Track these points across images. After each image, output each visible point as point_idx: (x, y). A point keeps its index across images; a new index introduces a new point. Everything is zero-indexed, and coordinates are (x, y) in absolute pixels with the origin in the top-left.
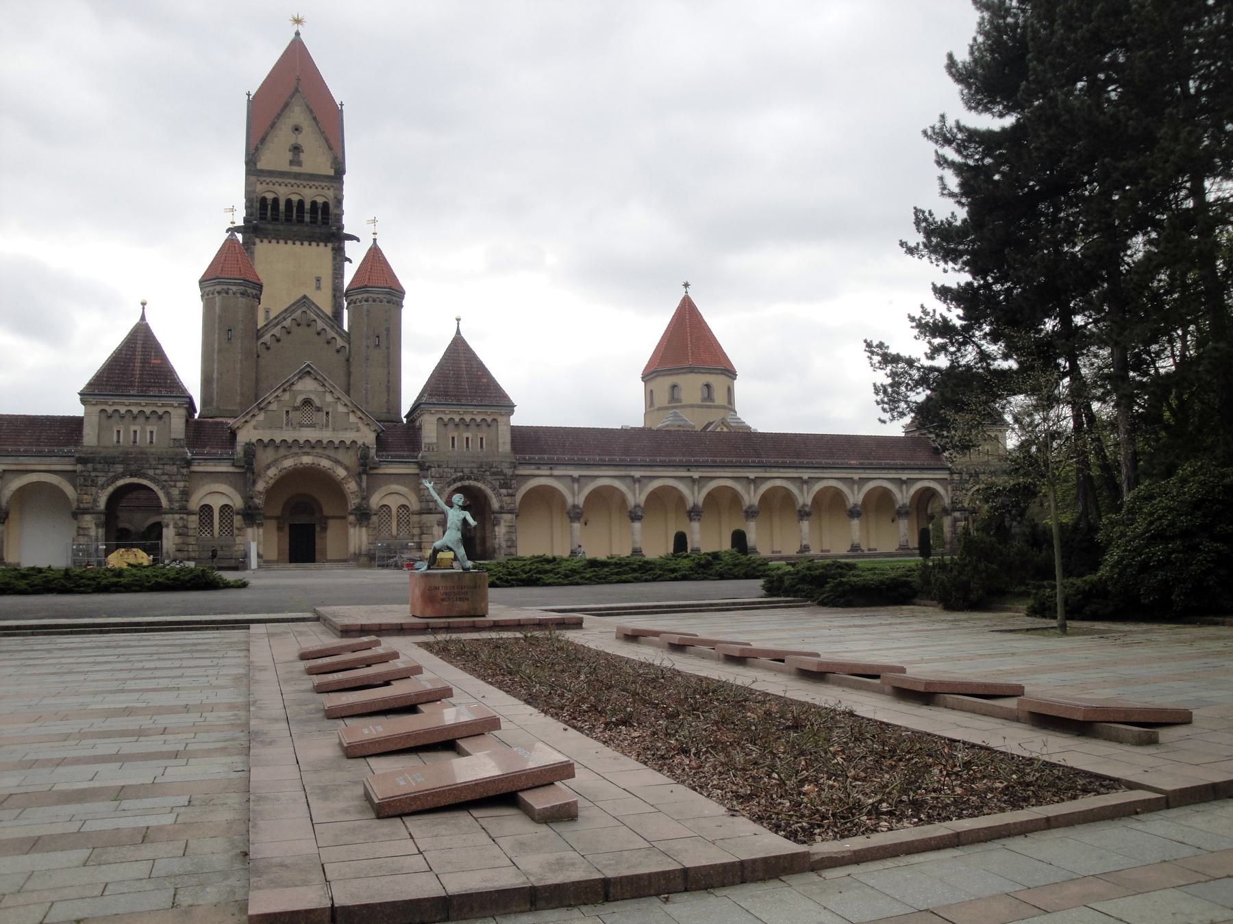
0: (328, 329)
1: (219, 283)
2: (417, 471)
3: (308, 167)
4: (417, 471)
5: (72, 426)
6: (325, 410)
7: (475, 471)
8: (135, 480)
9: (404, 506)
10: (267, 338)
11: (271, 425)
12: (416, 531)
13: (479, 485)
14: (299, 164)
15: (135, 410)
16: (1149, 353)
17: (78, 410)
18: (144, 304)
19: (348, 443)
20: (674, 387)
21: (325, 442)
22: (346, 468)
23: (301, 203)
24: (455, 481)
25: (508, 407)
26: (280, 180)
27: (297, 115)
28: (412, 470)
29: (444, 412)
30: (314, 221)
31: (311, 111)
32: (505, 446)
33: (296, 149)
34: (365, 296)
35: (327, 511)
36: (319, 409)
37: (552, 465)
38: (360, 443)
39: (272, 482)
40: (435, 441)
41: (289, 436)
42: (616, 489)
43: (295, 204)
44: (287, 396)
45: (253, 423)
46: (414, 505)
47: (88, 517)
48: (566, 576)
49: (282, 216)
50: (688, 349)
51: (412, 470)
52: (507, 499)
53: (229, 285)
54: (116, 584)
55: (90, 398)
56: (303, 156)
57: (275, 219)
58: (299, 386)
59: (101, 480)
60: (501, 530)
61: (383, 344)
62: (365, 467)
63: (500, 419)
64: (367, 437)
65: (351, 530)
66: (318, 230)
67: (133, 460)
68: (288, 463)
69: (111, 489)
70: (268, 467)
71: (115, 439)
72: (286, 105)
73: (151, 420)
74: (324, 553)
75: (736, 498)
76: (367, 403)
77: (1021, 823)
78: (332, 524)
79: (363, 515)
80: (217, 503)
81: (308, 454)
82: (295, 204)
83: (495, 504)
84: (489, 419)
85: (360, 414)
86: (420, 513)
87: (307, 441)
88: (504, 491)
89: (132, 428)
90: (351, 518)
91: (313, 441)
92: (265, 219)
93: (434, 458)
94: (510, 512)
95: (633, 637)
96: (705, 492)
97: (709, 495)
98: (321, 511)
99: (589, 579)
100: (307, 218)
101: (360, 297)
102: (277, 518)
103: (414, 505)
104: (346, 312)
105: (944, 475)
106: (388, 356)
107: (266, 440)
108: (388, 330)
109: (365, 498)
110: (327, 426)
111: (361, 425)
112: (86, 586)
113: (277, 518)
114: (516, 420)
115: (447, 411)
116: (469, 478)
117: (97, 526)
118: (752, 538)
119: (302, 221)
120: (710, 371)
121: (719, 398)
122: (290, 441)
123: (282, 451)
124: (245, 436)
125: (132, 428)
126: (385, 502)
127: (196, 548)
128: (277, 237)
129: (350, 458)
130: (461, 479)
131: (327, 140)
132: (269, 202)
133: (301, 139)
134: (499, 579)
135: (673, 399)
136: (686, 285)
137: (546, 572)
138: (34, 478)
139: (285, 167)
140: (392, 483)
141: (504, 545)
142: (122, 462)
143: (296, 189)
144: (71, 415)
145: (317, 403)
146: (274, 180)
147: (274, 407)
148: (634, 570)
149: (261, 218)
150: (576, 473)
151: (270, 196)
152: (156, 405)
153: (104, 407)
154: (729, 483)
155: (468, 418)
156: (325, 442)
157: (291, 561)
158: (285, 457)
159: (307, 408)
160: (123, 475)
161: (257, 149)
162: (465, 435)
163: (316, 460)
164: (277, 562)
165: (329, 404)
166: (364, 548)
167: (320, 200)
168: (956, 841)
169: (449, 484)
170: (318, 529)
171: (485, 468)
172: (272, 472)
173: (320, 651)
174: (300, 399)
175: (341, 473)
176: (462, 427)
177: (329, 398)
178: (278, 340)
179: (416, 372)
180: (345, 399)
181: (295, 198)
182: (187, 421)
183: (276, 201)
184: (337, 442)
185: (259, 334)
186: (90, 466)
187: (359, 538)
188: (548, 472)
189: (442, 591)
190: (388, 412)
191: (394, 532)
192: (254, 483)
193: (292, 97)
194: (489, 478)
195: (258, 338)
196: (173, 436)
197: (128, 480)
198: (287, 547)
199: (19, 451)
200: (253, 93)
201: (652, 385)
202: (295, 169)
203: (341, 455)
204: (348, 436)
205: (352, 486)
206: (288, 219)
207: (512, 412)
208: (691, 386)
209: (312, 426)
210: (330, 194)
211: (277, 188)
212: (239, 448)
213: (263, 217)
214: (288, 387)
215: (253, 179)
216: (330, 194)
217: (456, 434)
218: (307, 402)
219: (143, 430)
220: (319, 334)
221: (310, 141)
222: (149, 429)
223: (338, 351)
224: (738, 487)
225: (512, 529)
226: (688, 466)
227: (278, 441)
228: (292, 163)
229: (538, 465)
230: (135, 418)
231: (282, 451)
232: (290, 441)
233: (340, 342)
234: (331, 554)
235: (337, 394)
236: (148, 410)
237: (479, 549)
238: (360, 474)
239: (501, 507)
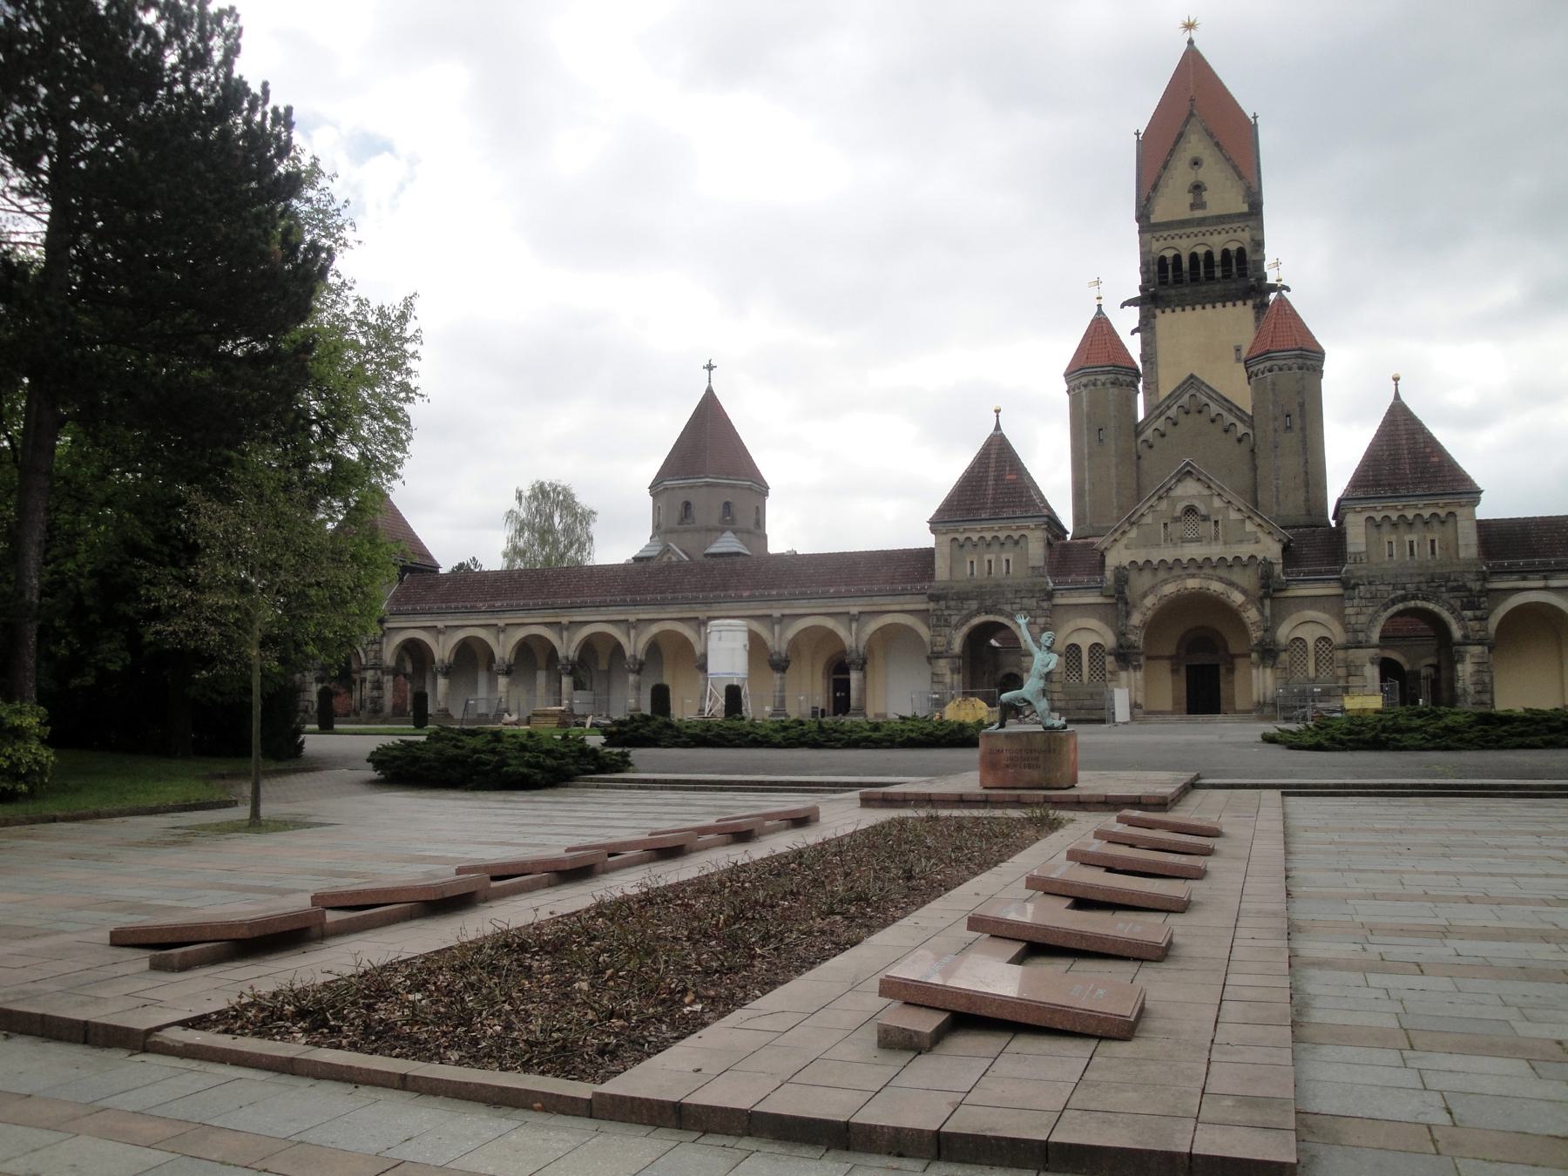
0: (1225, 414)
1: (1085, 374)
2: (1340, 591)
3: (1213, 209)
4: (1340, 591)
5: (923, 559)
6: (1213, 518)
7: (1424, 587)
8: (991, 618)
9: (1324, 638)
12: (1341, 672)
13: (1431, 606)
15: (988, 536)
16: (322, 451)
17: (927, 540)
18: (1396, 379)
19: (1245, 559)
21: (1214, 559)
22: (1244, 592)
23: (1209, 254)
24: (1393, 602)
25: (1470, 493)
26: (1180, 232)
27: (1195, 145)
28: (1333, 589)
29: (1374, 509)
30: (1227, 275)
31: (1211, 136)
32: (1469, 546)
33: (1197, 188)
34: (1268, 364)
35: (1234, 648)
36: (1205, 518)
37: (1547, 572)
38: (1260, 557)
39: (1150, 613)
40: (1363, 548)
41: (1169, 554)
42: (656, 636)
43: (1202, 258)
44: (1164, 505)
45: (1124, 541)
46: (1338, 635)
47: (942, 662)
48: (1435, 736)
49: (1186, 276)
51: (1333, 589)
52: (1475, 625)
53: (1098, 369)
54: (867, 739)
55: (940, 527)
56: (1206, 196)
57: (1178, 280)
58: (1179, 491)
59: (954, 620)
60: (1465, 671)
61: (1297, 427)
62: (1269, 590)
63: (1459, 511)
64: (1271, 549)
65: (1254, 672)
66: (1233, 286)
67: (987, 595)
68: (1169, 589)
69: (965, 629)
70: (1145, 596)
71: (969, 571)
72: (1181, 135)
74: (1232, 702)
76: (1278, 504)
77: (369, 1071)
78: (1239, 662)
79: (1269, 653)
80: (1085, 641)
81: (1193, 576)
82: (1202, 258)
83: (1457, 633)
84: (1442, 513)
85: (1259, 520)
86: (1346, 648)
87: (1192, 560)
88: (1469, 613)
89: (987, 557)
90: (1254, 656)
91: (1200, 559)
92: (1165, 283)
93: (1363, 572)
94: (1480, 643)
95: (800, 821)
98: (1226, 648)
99: (1470, 741)
100: (1218, 273)
101: (1261, 366)
102: (1170, 658)
103: (1338, 635)
104: (1140, 398)
106: (1304, 442)
107: (1141, 562)
108: (1302, 405)
109: (1270, 629)
110: (1216, 538)
111: (1261, 535)
112: (839, 740)
113: (1170, 658)
114: (1483, 512)
115: (1379, 505)
116: (1415, 597)
117: (953, 671)
119: (1213, 278)
122: (1170, 560)
123: (1162, 574)
124: (1117, 557)
125: (987, 557)
126: (1298, 634)
127: (1062, 696)
128: (1182, 303)
129: (1248, 579)
130: (1404, 599)
131: (1235, 167)
132: (1169, 262)
133: (1203, 175)
134: (1333, 739)
136: (710, 367)
137: (1410, 730)
138: (888, 619)
140: (1311, 608)
141: (1471, 689)
143: (1201, 239)
144: (1522, 516)
145: (1203, 510)
146: (1172, 233)
147: (1148, 519)
148: (1553, 730)
149: (1161, 283)
151: (1169, 254)
152: (1010, 528)
153: (1373, 514)
155: (1410, 514)
156: (1214, 559)
157: (1190, 712)
158: (1165, 581)
159: (1191, 518)
160: (978, 613)
161: (1148, 199)
162: (1408, 538)
163: (1205, 583)
164: (1172, 713)
165: (1218, 511)
166: (1269, 694)
167: (1233, 247)
168: (404, 1083)
169: (1386, 607)
170: (1222, 670)
171: (1436, 583)
172: (1149, 601)
173: (1196, 827)
174: (1180, 507)
175: (1237, 598)
176: (1402, 528)
177: (1217, 503)
178: (1163, 435)
179: (1345, 448)
181: (1201, 250)
182: (1049, 544)
183: (1177, 258)
184: (1230, 559)
185: (1138, 429)
186: (942, 603)
188: (1541, 584)
189: (1006, 755)
190: (1309, 513)
191: (1312, 673)
192: (1128, 615)
193: (1187, 122)
194: (1445, 596)
195: (1138, 435)
196: (1031, 564)
197: (983, 618)
198: (1184, 694)
199: (1502, 566)
200: (1142, 131)
202: (1199, 214)
203: (1237, 576)
204: (1244, 551)
205: (1251, 615)
206: (1195, 278)
207: (1476, 502)
209: (1198, 540)
211: (1177, 239)
212: (1109, 574)
213: (1163, 281)
214: (1164, 493)
215: (1148, 236)
216: (1245, 236)
217: (1393, 538)
218: (1190, 510)
219: (998, 560)
220: (1213, 421)
221: (1214, 174)
222: (1004, 557)
223: (1240, 440)
224: (616, 632)
225: (1482, 667)
227: (1155, 562)
228: (1193, 206)
229: (1524, 574)
230: (989, 545)
231: (1162, 574)
232: (1170, 560)
233: (1241, 429)
234: (1239, 705)
235: (1227, 497)
236: (1002, 535)
237: (1445, 695)
238: (1261, 599)
239: (1466, 637)
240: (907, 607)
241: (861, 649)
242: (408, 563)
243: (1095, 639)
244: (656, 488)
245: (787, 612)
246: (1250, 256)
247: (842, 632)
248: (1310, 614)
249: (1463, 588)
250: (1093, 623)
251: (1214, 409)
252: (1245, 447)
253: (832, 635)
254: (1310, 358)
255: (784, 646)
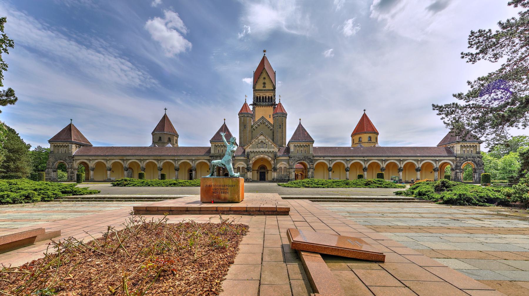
3: (267, 88)
5: (210, 148)
10: (254, 127)
11: (253, 147)
14: (265, 87)
17: (209, 145)
20: (360, 138)
27: (264, 75)
33: (264, 83)
41: (257, 150)
44: (257, 140)
50: (365, 127)
51: (288, 158)
56: (266, 85)
58: (260, 138)
68: (257, 157)
75: (378, 165)
79: (275, 169)
83: (309, 167)
96: (369, 163)
97: (370, 164)
105: (454, 158)
109: (276, 164)
118: (277, 150)
120: (371, 133)
121: (373, 140)
135: (360, 141)
136: (166, 109)
138: (201, 161)
139: (262, 88)
145: (264, 142)
147: (254, 143)
150: (330, 159)
151: (259, 96)
154: (376, 161)
171: (306, 158)
174: (260, 141)
175: (270, 159)
177: (267, 141)
179: (290, 134)
180: (271, 141)
181: (264, 96)
187: (275, 175)
201: (353, 138)
202: (264, 89)
203: (270, 155)
204: (272, 150)
205: (272, 162)
208: (365, 137)
209: (263, 147)
210: (272, 94)
218: (262, 142)
221: (267, 81)
224: (379, 162)
226: (364, 157)
233: (271, 128)
242: (282, 259)
243: (243, 166)
244: (153, 133)
246: (273, 98)
247: (191, 163)
248: (283, 162)
249: (310, 159)
250: (242, 163)
251: (267, 123)
252: (272, 131)
253: (189, 163)
254: (285, 115)
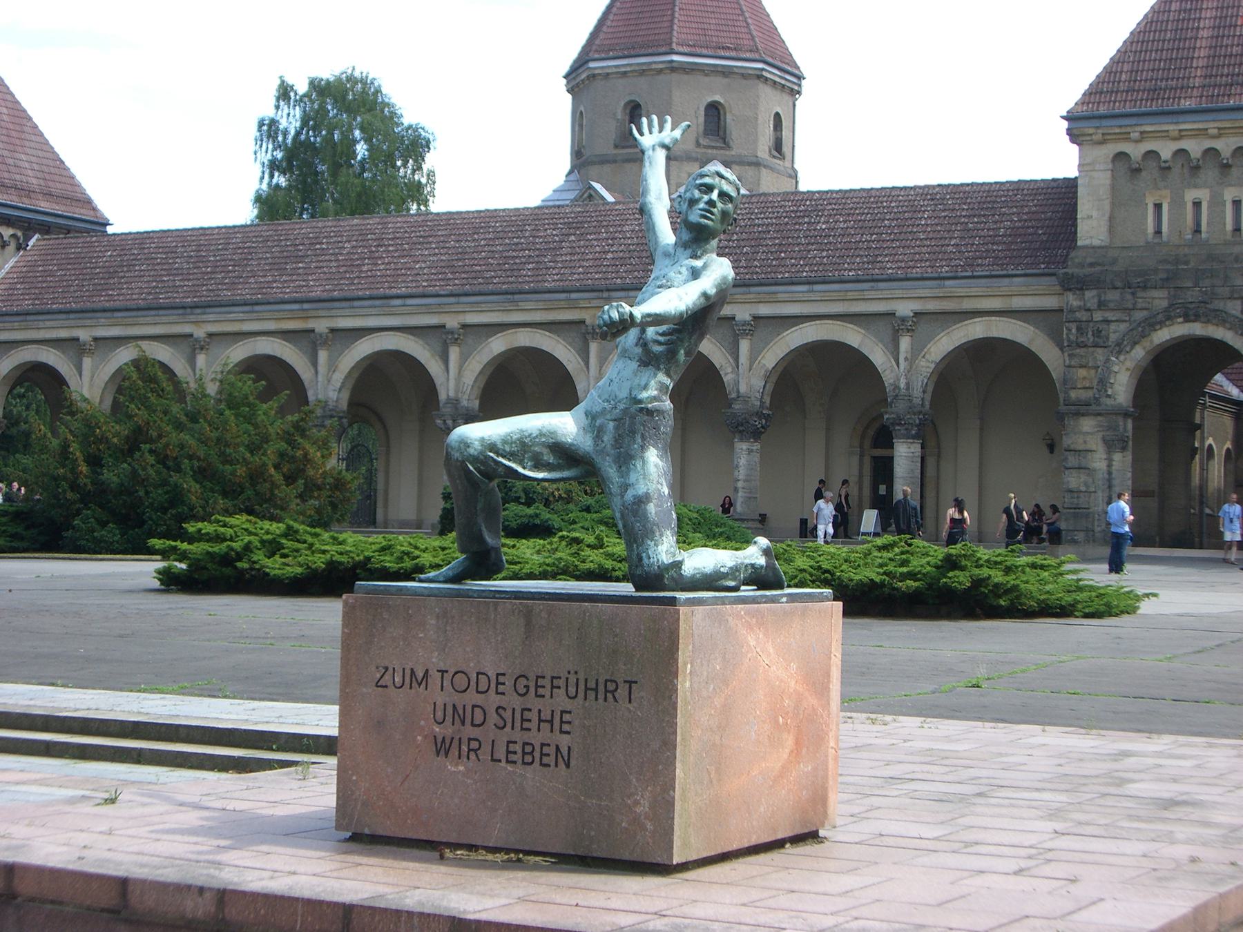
5: (1061, 195)
59: (1116, 331)
69: (1139, 353)
73: (1235, 172)
138: (976, 330)
142: (1165, 283)
160: (1168, 317)
240: (1018, 303)
241: (917, 392)
245: (764, 310)
247: (878, 356)
255: (758, 383)
